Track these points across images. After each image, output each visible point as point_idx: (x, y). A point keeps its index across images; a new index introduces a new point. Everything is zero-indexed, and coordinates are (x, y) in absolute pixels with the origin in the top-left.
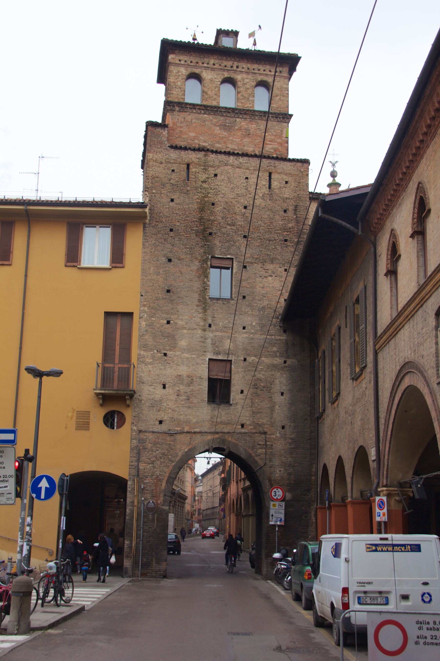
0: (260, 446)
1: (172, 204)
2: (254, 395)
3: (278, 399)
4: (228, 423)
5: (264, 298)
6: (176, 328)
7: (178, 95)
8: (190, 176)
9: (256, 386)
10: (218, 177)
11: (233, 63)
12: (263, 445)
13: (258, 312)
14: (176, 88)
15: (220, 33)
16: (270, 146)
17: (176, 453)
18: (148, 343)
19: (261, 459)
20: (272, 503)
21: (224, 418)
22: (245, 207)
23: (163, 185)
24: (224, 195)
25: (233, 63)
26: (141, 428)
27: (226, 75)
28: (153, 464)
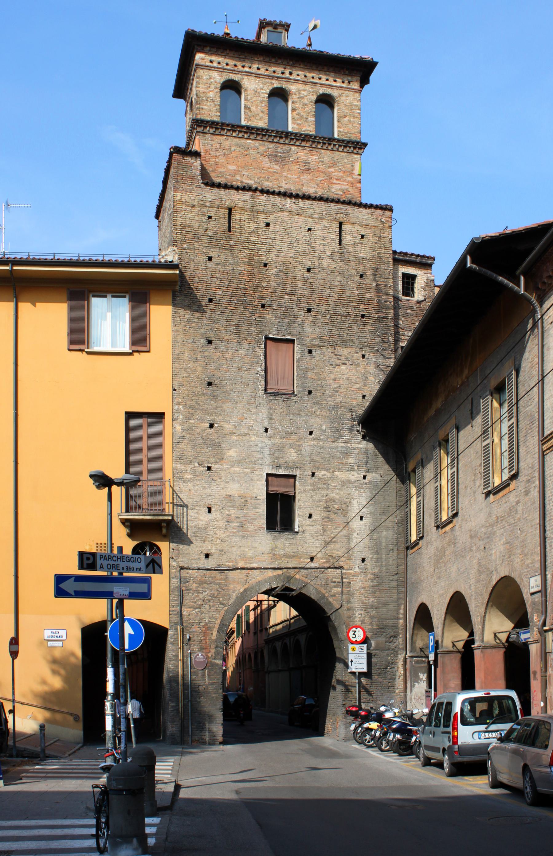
0: (335, 584)
1: (209, 264)
2: (326, 520)
3: (356, 524)
4: (294, 556)
5: (337, 394)
6: (222, 433)
7: (210, 110)
9: (327, 509)
12: (338, 582)
13: (328, 412)
14: (207, 100)
15: (263, 25)
16: (338, 187)
17: (229, 595)
18: (185, 453)
19: (336, 600)
21: (289, 550)
22: (309, 270)
23: (197, 238)
24: (280, 252)
28: (200, 608)
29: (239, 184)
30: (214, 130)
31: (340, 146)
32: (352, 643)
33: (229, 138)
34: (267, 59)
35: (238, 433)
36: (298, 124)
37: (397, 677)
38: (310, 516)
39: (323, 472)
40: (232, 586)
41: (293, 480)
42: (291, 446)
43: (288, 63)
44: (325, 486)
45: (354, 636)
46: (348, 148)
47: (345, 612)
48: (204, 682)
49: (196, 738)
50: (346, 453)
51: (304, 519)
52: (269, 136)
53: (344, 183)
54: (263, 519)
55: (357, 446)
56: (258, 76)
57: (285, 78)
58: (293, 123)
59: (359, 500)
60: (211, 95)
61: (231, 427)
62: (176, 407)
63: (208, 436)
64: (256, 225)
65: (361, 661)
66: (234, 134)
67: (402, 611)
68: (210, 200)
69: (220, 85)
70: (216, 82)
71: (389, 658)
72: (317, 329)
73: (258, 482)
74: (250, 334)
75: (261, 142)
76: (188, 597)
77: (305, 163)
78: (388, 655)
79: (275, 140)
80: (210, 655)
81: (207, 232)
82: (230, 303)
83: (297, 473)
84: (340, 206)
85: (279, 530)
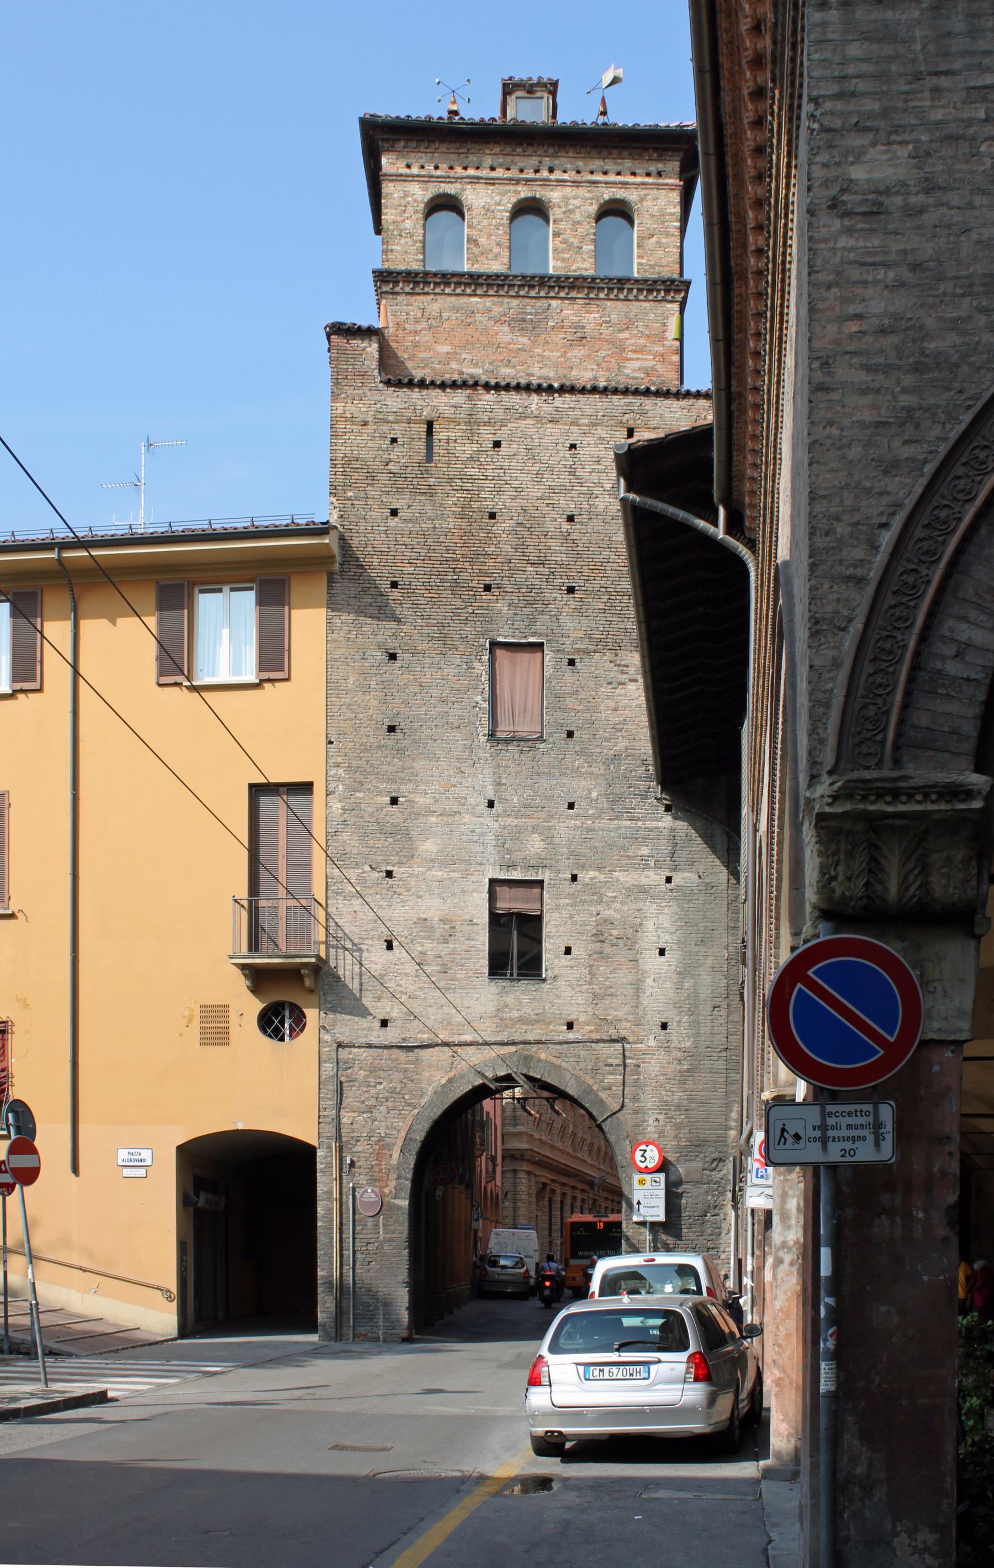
0: (611, 1068)
1: (393, 522)
2: (596, 956)
3: (652, 963)
4: (537, 1022)
5: (619, 734)
6: (412, 813)
7: (406, 252)
8: (436, 450)
9: (599, 937)
10: (504, 449)
11: (541, 162)
12: (617, 1065)
13: (603, 768)
14: (400, 235)
15: (509, 88)
16: (636, 364)
17: (421, 1089)
18: (348, 849)
19: (613, 1096)
20: (637, 1177)
21: (528, 1011)
22: (571, 519)
23: (372, 477)
24: (518, 490)
25: (541, 162)
26: (341, 1038)
27: (524, 192)
28: (371, 1112)
29: (456, 377)
30: (411, 286)
31: (640, 290)
32: (641, 1171)
33: (439, 297)
34: (508, 150)
35: (439, 811)
36: (563, 260)
37: (724, 1232)
38: (568, 951)
39: (592, 873)
40: (427, 1074)
41: (538, 890)
42: (535, 830)
43: (546, 152)
44: (595, 898)
45: (643, 1159)
46: (655, 294)
47: (629, 1117)
48: (376, 1236)
49: (362, 1330)
50: (635, 838)
51: (557, 957)
52: (510, 286)
53: (648, 357)
54: (483, 958)
55: (655, 824)
56: (491, 182)
57: (541, 180)
58: (554, 258)
59: (659, 923)
60: (408, 224)
61: (428, 801)
62: (332, 772)
63: (388, 818)
64: (475, 447)
65: (654, 1202)
66: (447, 291)
67: (734, 1115)
68: (395, 410)
69: (423, 205)
70: (415, 201)
71: (709, 1198)
72: (585, 621)
73: (475, 895)
74: (464, 639)
75: (495, 299)
76: (351, 1093)
77: (575, 328)
78: (707, 1192)
79: (522, 293)
80: (386, 1191)
81: (389, 467)
82: (428, 587)
83: (545, 876)
84: (630, 399)
85: (515, 976)
